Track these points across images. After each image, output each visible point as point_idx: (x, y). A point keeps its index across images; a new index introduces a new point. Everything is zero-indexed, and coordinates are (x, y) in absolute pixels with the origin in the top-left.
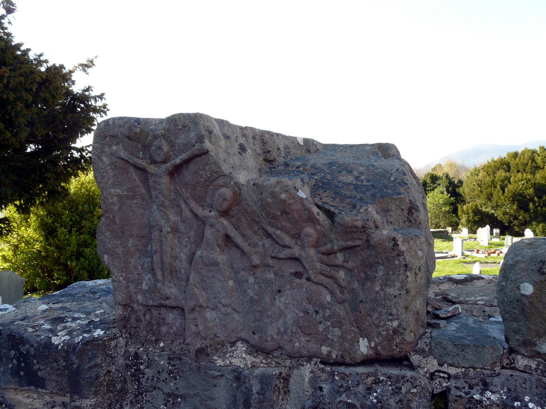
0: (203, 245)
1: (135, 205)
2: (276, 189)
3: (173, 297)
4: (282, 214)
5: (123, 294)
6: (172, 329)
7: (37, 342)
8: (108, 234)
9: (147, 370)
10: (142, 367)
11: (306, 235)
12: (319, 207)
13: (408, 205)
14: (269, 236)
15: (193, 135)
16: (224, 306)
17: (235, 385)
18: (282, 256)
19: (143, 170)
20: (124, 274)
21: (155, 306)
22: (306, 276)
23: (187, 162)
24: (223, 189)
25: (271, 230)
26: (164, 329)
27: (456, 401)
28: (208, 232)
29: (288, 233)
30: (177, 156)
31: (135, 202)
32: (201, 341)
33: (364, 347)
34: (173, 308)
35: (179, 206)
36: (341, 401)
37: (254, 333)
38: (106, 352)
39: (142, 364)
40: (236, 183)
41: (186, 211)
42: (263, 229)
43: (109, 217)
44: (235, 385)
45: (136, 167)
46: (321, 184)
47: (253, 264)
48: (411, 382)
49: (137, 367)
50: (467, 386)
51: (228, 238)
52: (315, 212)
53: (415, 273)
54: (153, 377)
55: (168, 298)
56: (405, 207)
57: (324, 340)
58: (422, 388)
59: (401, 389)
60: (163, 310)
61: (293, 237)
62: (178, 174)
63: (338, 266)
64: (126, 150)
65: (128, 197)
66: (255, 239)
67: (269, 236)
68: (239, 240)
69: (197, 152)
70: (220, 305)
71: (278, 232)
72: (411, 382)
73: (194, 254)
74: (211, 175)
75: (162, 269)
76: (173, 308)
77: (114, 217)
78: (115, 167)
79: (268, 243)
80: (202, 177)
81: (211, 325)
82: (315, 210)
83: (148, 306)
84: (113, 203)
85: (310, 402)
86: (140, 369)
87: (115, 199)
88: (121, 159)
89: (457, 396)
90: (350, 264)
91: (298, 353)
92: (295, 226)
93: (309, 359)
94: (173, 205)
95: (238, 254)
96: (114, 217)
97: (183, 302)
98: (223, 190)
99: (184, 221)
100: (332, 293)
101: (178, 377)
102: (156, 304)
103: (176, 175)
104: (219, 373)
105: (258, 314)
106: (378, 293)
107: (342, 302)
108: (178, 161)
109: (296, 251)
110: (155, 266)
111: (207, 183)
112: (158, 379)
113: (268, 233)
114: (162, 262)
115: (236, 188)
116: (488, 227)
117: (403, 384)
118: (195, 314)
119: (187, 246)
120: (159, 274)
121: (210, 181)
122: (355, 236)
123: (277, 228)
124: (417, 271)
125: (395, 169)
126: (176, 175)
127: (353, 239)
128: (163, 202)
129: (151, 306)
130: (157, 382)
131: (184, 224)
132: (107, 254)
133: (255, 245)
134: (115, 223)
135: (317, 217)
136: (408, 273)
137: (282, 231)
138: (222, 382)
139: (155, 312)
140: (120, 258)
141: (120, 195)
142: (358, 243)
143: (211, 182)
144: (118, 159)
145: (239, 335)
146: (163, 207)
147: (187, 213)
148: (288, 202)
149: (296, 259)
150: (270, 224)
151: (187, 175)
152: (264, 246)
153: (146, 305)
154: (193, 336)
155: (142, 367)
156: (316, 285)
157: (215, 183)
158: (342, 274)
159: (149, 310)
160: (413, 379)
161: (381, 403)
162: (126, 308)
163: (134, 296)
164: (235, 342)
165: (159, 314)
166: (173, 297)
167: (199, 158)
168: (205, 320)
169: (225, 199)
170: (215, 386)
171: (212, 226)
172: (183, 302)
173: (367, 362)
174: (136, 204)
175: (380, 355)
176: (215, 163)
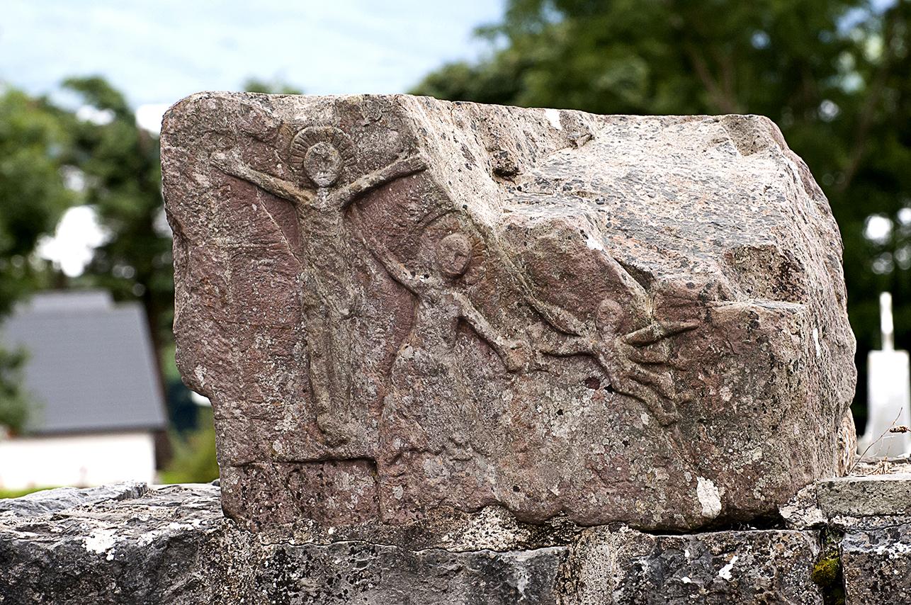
0: (413, 337)
1: (265, 268)
2: (551, 236)
3: (354, 439)
4: (562, 277)
5: (242, 442)
6: (350, 501)
7: (49, 553)
8: (207, 326)
9: (304, 581)
10: (293, 576)
11: (605, 313)
12: (624, 266)
13: (782, 260)
14: (539, 316)
15: (393, 136)
16: (458, 445)
17: (483, 584)
18: (563, 350)
19: (289, 202)
20: (244, 404)
21: (313, 461)
22: (606, 383)
23: (379, 187)
24: (455, 235)
25: (541, 305)
26: (331, 503)
27: (852, 560)
28: (426, 314)
29: (572, 310)
30: (359, 175)
31: (266, 261)
32: (414, 515)
33: (709, 499)
34: (350, 460)
35: (363, 269)
36: (673, 583)
37: (516, 489)
38: (209, 559)
39: (293, 570)
40: (478, 226)
41: (379, 277)
42: (529, 304)
43: (210, 292)
44: (483, 584)
45: (269, 192)
46: (618, 223)
47: (511, 367)
48: (783, 541)
49: (284, 577)
50: (867, 539)
51: (462, 323)
52: (620, 274)
53: (788, 371)
54: (318, 592)
55: (343, 442)
56: (776, 265)
57: (640, 491)
58: (801, 548)
59: (768, 553)
60: (329, 469)
61: (582, 316)
62: (360, 208)
63: (660, 364)
64: (246, 159)
65: (251, 254)
66: (515, 323)
67: (539, 316)
68: (482, 325)
69: (403, 169)
70: (451, 444)
71: (556, 310)
72: (783, 541)
73: (394, 355)
74: (431, 211)
75: (331, 388)
76: (350, 460)
77: (223, 292)
78: (223, 194)
79: (536, 329)
80: (412, 215)
81: (432, 482)
82: (620, 271)
83: (296, 462)
84: (221, 263)
85: (619, 592)
86: (290, 581)
87: (225, 256)
88: (239, 178)
89: (851, 553)
90: (682, 360)
91: (594, 516)
92: (586, 299)
93: (614, 526)
94: (350, 265)
95: (477, 352)
96: (223, 292)
97: (375, 447)
98: (453, 237)
99: (374, 296)
100: (650, 410)
101: (370, 586)
102: (317, 456)
103: (355, 210)
104: (454, 567)
105: (521, 454)
106: (727, 404)
107: (668, 425)
108: (364, 183)
109: (588, 341)
110: (315, 382)
111: (421, 225)
112: (329, 593)
113: (536, 312)
114: (331, 373)
115: (478, 234)
116: (150, 120)
117: (771, 547)
118: (400, 466)
119: (380, 343)
120: (324, 398)
121: (427, 221)
122: (687, 312)
123: (554, 302)
124: (791, 368)
125: (762, 187)
126: (355, 210)
127: (685, 318)
128: (333, 262)
129: (305, 462)
130: (326, 600)
131: (374, 302)
132: (204, 364)
133: (512, 335)
134: (225, 304)
135: (623, 281)
136: (775, 370)
137: (562, 307)
138: (459, 580)
139: (312, 474)
140: (237, 372)
141: (234, 249)
142: (691, 323)
143: (429, 223)
144: (230, 178)
145: (488, 495)
146: (334, 271)
147: (380, 279)
148: (574, 257)
149: (589, 356)
150: (540, 296)
151: (381, 209)
152: (529, 334)
153: (293, 462)
154: (398, 507)
155: (293, 576)
156: (624, 397)
157: (437, 225)
158: (666, 378)
159: (296, 470)
160: (787, 537)
161: (737, 577)
162: (246, 472)
163: (264, 445)
164: (480, 509)
165: (320, 476)
166: (354, 439)
167: (405, 180)
168: (421, 474)
169: (458, 254)
170: (445, 591)
171: (433, 302)
172: (375, 447)
173: (710, 525)
174: (269, 265)
175: (735, 509)
176: (438, 189)
